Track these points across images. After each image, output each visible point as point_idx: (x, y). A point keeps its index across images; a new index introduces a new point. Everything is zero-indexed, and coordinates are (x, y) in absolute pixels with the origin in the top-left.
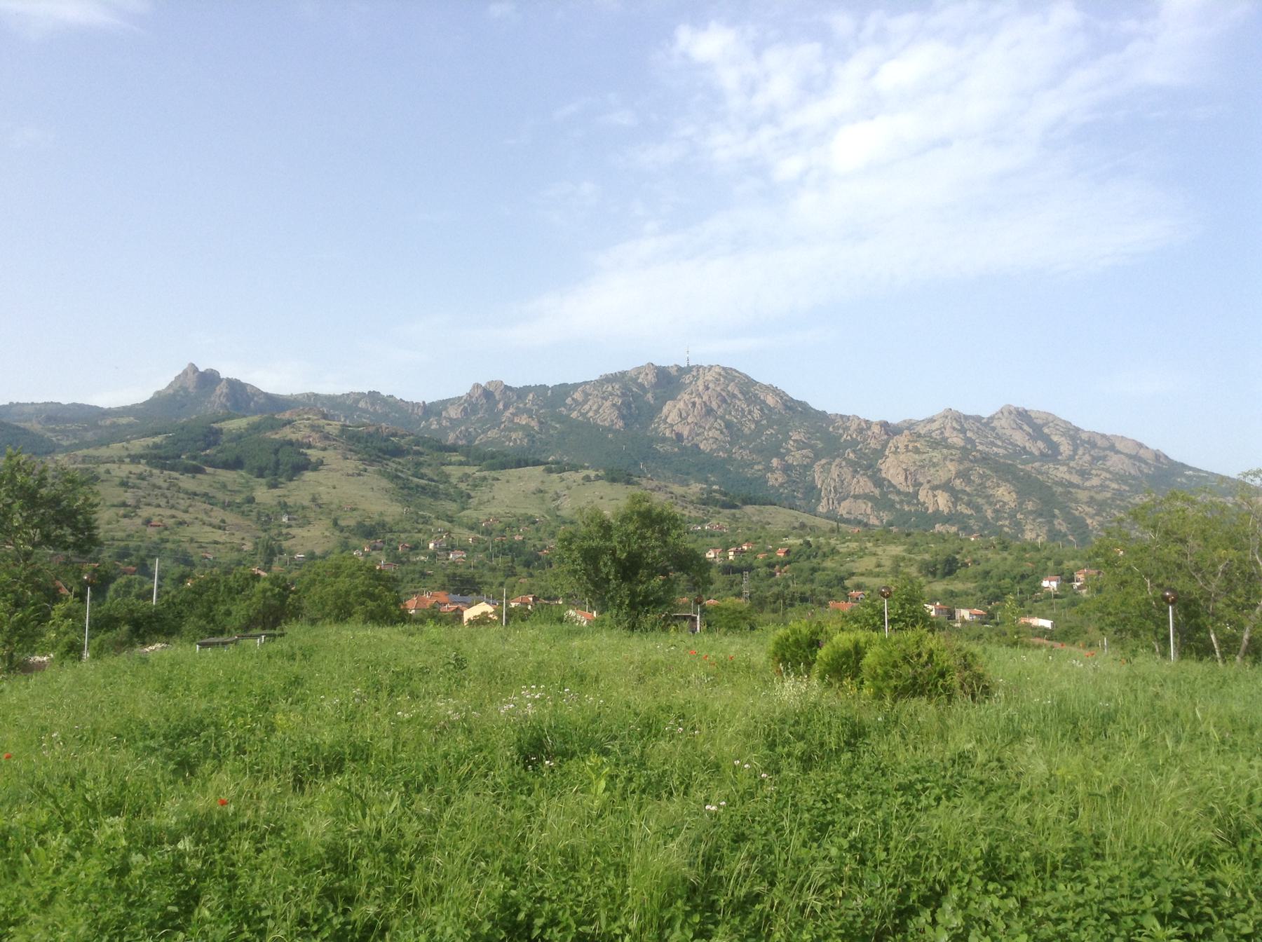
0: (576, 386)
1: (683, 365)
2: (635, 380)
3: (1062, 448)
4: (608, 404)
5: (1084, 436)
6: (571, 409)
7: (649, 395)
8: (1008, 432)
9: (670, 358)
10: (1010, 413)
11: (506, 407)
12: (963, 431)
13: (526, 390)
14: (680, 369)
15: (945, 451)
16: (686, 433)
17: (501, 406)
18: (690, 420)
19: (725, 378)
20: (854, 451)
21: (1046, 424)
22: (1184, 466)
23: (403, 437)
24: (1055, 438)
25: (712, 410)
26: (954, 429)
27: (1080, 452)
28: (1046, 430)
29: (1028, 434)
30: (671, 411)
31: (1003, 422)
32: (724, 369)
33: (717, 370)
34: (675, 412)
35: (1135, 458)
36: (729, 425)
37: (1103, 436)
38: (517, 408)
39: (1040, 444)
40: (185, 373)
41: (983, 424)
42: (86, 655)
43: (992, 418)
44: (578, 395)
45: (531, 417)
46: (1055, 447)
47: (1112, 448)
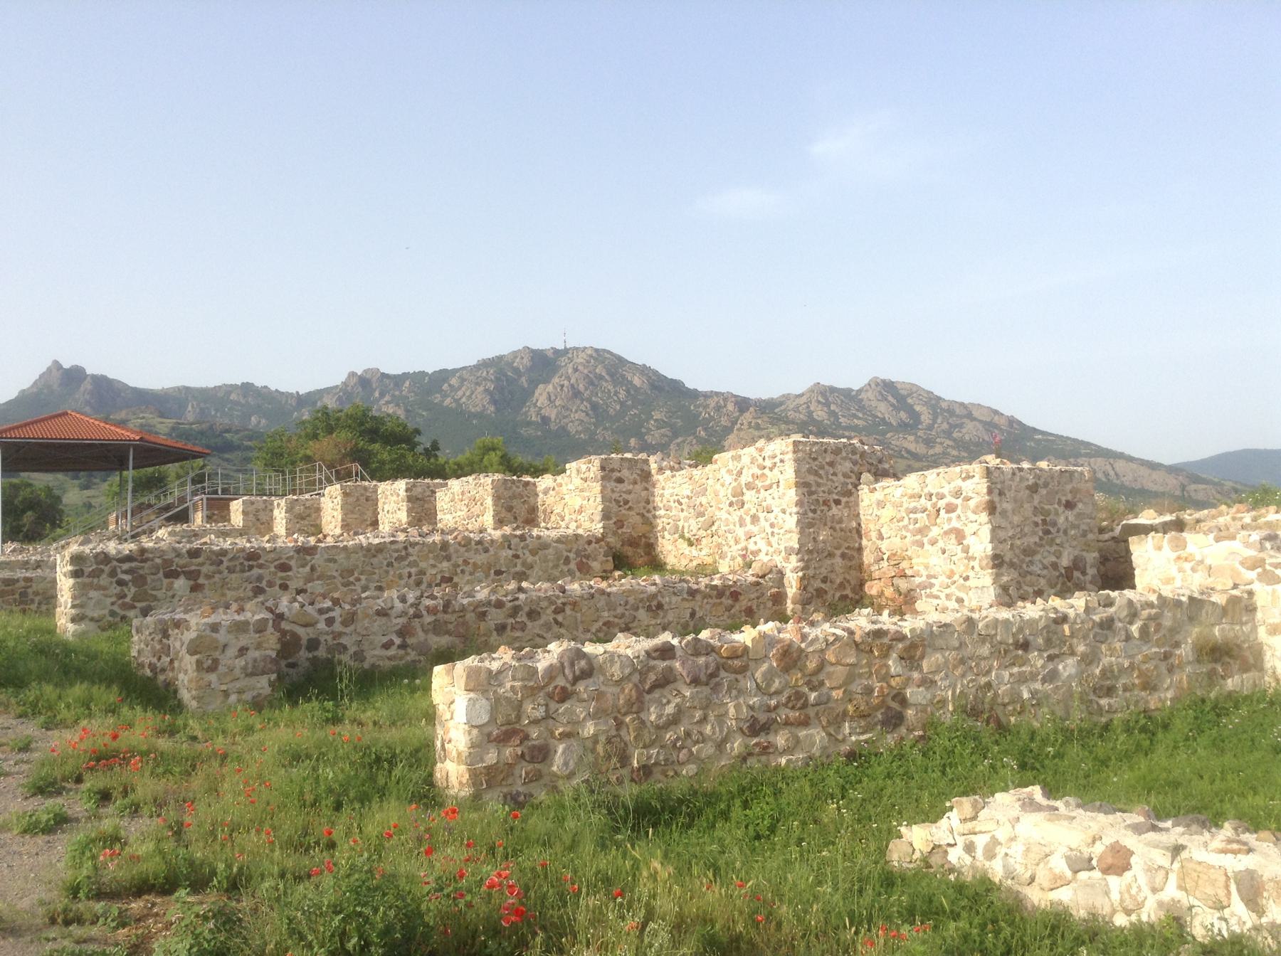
0: (455, 371)
1: (560, 347)
2: (510, 364)
3: (923, 417)
4: (481, 389)
5: (944, 405)
6: (445, 396)
7: (523, 379)
8: (874, 404)
9: (545, 341)
10: (877, 384)
11: (382, 395)
12: (827, 404)
13: (405, 376)
14: (556, 351)
15: (783, 426)
16: (553, 417)
17: (377, 394)
18: (557, 403)
19: (596, 359)
20: (705, 430)
21: (909, 395)
22: (1035, 430)
23: (237, 432)
24: (917, 408)
25: (579, 392)
26: (819, 402)
27: (939, 421)
28: (909, 401)
29: (892, 405)
30: (541, 395)
31: (870, 395)
32: (597, 350)
33: (589, 352)
34: (545, 395)
35: (990, 426)
36: (595, 407)
37: (962, 404)
38: (393, 396)
39: (903, 415)
40: (49, 370)
41: (848, 396)
42: (282, 725)
43: (860, 391)
44: (454, 381)
45: (398, 405)
46: (915, 416)
47: (970, 416)
